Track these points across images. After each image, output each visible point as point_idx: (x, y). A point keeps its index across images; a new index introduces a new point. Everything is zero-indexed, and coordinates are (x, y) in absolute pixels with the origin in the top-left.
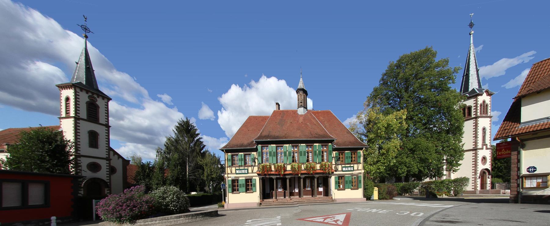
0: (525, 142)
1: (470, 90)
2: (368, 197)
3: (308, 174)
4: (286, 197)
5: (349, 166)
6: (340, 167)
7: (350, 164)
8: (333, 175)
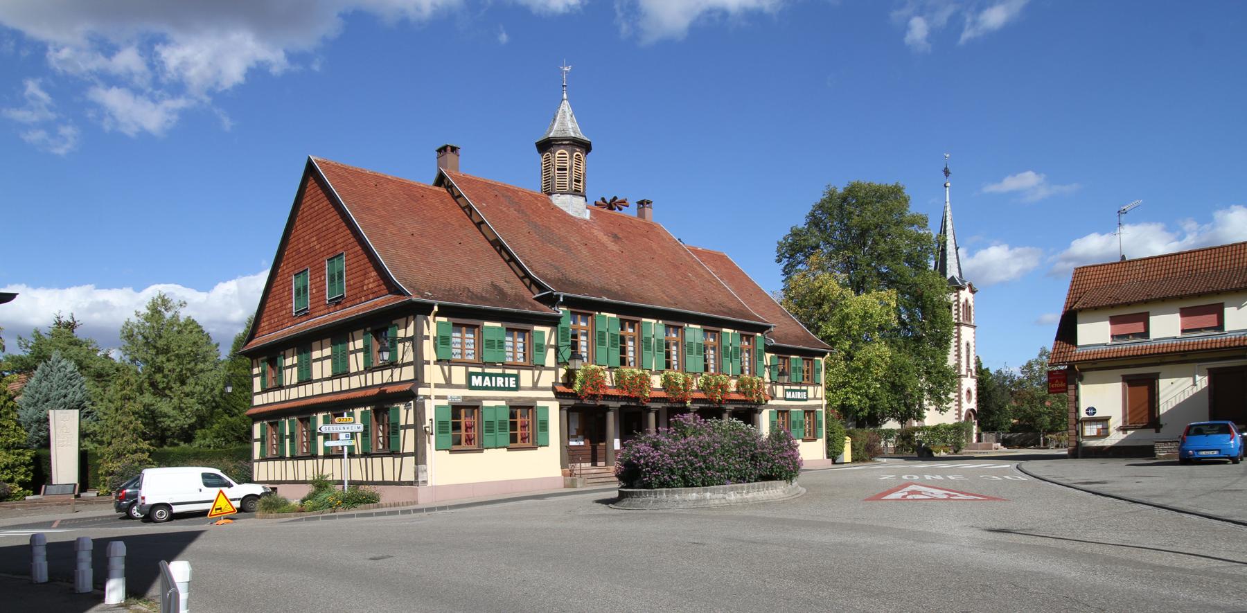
0: (1083, 373)
1: (949, 276)
2: (833, 454)
3: (711, 401)
4: (599, 464)
5: (798, 388)
6: (779, 390)
7: (800, 384)
8: (766, 408)
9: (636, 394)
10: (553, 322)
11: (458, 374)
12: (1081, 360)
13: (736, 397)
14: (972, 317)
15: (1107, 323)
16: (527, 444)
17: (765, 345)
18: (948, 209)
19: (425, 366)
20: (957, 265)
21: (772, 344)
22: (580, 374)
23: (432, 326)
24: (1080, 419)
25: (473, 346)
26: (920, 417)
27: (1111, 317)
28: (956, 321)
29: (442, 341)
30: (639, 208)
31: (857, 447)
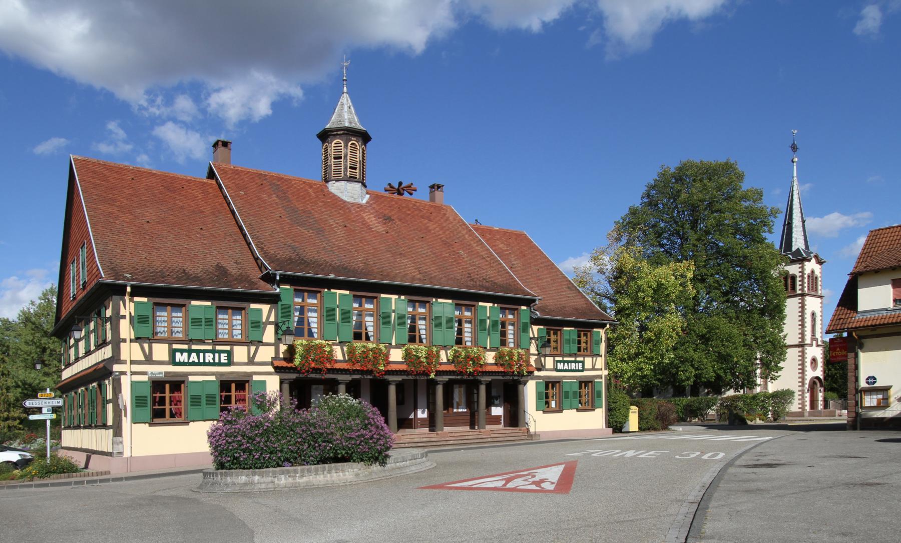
0: (863, 341)
1: (794, 249)
7: (575, 355)
8: (532, 379)
9: (370, 367)
10: (272, 299)
11: (161, 351)
12: (860, 327)
13: (495, 368)
14: (819, 288)
15: (890, 287)
16: (176, 420)
17: (531, 318)
18: (795, 184)
19: (122, 344)
20: (803, 238)
21: (536, 317)
22: (299, 350)
23: (128, 307)
24: (860, 388)
25: (240, 326)
26: (751, 384)
27: (893, 280)
28: (800, 292)
29: (139, 320)
30: (431, 192)
31: (645, 414)
